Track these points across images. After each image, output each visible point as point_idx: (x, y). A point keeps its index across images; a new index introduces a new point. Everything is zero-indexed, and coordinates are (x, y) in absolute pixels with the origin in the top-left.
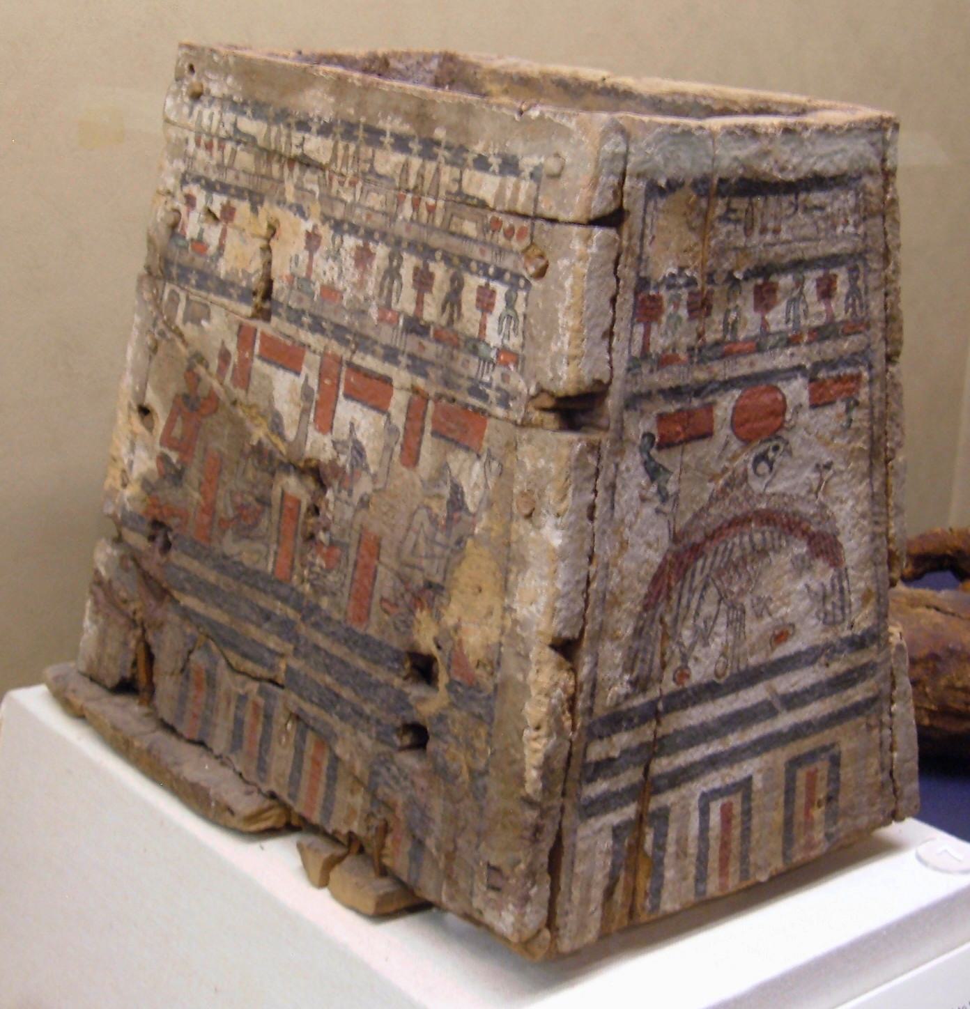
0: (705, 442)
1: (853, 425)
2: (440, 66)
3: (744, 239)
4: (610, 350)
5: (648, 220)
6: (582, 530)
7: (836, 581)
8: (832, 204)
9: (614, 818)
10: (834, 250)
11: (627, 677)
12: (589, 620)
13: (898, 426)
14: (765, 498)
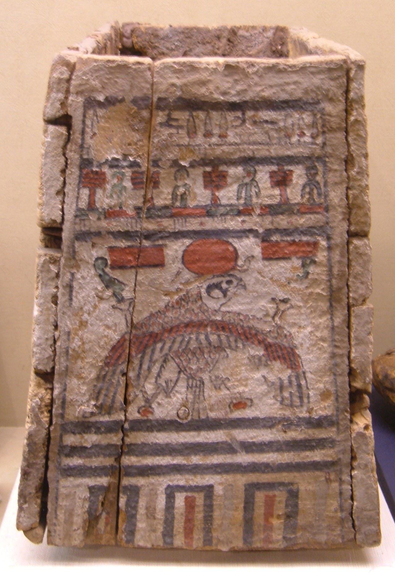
0: (157, 270)
1: (310, 277)
3: (188, 139)
4: (63, 202)
5: (88, 122)
6: (48, 309)
7: (293, 379)
8: (285, 120)
9: (91, 482)
10: (289, 153)
11: (93, 403)
12: (57, 363)
13: (362, 283)
14: (220, 313)
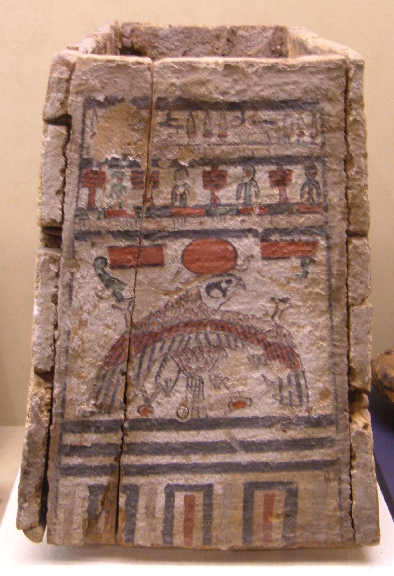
0: (157, 269)
1: (309, 276)
2: (274, 34)
3: (187, 139)
4: (63, 202)
5: (88, 122)
6: (48, 309)
7: (293, 378)
8: (284, 120)
9: (91, 481)
10: (288, 153)
11: (93, 402)
12: (57, 363)
13: (361, 282)
14: (220, 313)
